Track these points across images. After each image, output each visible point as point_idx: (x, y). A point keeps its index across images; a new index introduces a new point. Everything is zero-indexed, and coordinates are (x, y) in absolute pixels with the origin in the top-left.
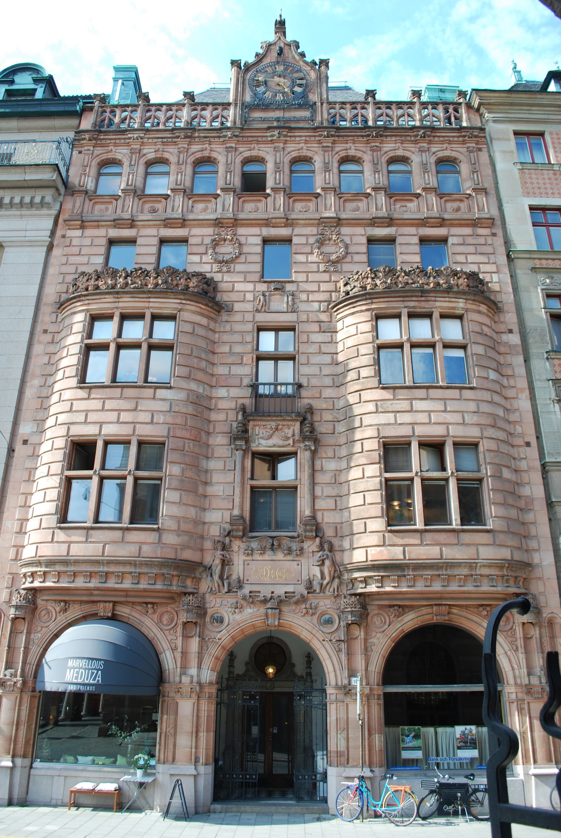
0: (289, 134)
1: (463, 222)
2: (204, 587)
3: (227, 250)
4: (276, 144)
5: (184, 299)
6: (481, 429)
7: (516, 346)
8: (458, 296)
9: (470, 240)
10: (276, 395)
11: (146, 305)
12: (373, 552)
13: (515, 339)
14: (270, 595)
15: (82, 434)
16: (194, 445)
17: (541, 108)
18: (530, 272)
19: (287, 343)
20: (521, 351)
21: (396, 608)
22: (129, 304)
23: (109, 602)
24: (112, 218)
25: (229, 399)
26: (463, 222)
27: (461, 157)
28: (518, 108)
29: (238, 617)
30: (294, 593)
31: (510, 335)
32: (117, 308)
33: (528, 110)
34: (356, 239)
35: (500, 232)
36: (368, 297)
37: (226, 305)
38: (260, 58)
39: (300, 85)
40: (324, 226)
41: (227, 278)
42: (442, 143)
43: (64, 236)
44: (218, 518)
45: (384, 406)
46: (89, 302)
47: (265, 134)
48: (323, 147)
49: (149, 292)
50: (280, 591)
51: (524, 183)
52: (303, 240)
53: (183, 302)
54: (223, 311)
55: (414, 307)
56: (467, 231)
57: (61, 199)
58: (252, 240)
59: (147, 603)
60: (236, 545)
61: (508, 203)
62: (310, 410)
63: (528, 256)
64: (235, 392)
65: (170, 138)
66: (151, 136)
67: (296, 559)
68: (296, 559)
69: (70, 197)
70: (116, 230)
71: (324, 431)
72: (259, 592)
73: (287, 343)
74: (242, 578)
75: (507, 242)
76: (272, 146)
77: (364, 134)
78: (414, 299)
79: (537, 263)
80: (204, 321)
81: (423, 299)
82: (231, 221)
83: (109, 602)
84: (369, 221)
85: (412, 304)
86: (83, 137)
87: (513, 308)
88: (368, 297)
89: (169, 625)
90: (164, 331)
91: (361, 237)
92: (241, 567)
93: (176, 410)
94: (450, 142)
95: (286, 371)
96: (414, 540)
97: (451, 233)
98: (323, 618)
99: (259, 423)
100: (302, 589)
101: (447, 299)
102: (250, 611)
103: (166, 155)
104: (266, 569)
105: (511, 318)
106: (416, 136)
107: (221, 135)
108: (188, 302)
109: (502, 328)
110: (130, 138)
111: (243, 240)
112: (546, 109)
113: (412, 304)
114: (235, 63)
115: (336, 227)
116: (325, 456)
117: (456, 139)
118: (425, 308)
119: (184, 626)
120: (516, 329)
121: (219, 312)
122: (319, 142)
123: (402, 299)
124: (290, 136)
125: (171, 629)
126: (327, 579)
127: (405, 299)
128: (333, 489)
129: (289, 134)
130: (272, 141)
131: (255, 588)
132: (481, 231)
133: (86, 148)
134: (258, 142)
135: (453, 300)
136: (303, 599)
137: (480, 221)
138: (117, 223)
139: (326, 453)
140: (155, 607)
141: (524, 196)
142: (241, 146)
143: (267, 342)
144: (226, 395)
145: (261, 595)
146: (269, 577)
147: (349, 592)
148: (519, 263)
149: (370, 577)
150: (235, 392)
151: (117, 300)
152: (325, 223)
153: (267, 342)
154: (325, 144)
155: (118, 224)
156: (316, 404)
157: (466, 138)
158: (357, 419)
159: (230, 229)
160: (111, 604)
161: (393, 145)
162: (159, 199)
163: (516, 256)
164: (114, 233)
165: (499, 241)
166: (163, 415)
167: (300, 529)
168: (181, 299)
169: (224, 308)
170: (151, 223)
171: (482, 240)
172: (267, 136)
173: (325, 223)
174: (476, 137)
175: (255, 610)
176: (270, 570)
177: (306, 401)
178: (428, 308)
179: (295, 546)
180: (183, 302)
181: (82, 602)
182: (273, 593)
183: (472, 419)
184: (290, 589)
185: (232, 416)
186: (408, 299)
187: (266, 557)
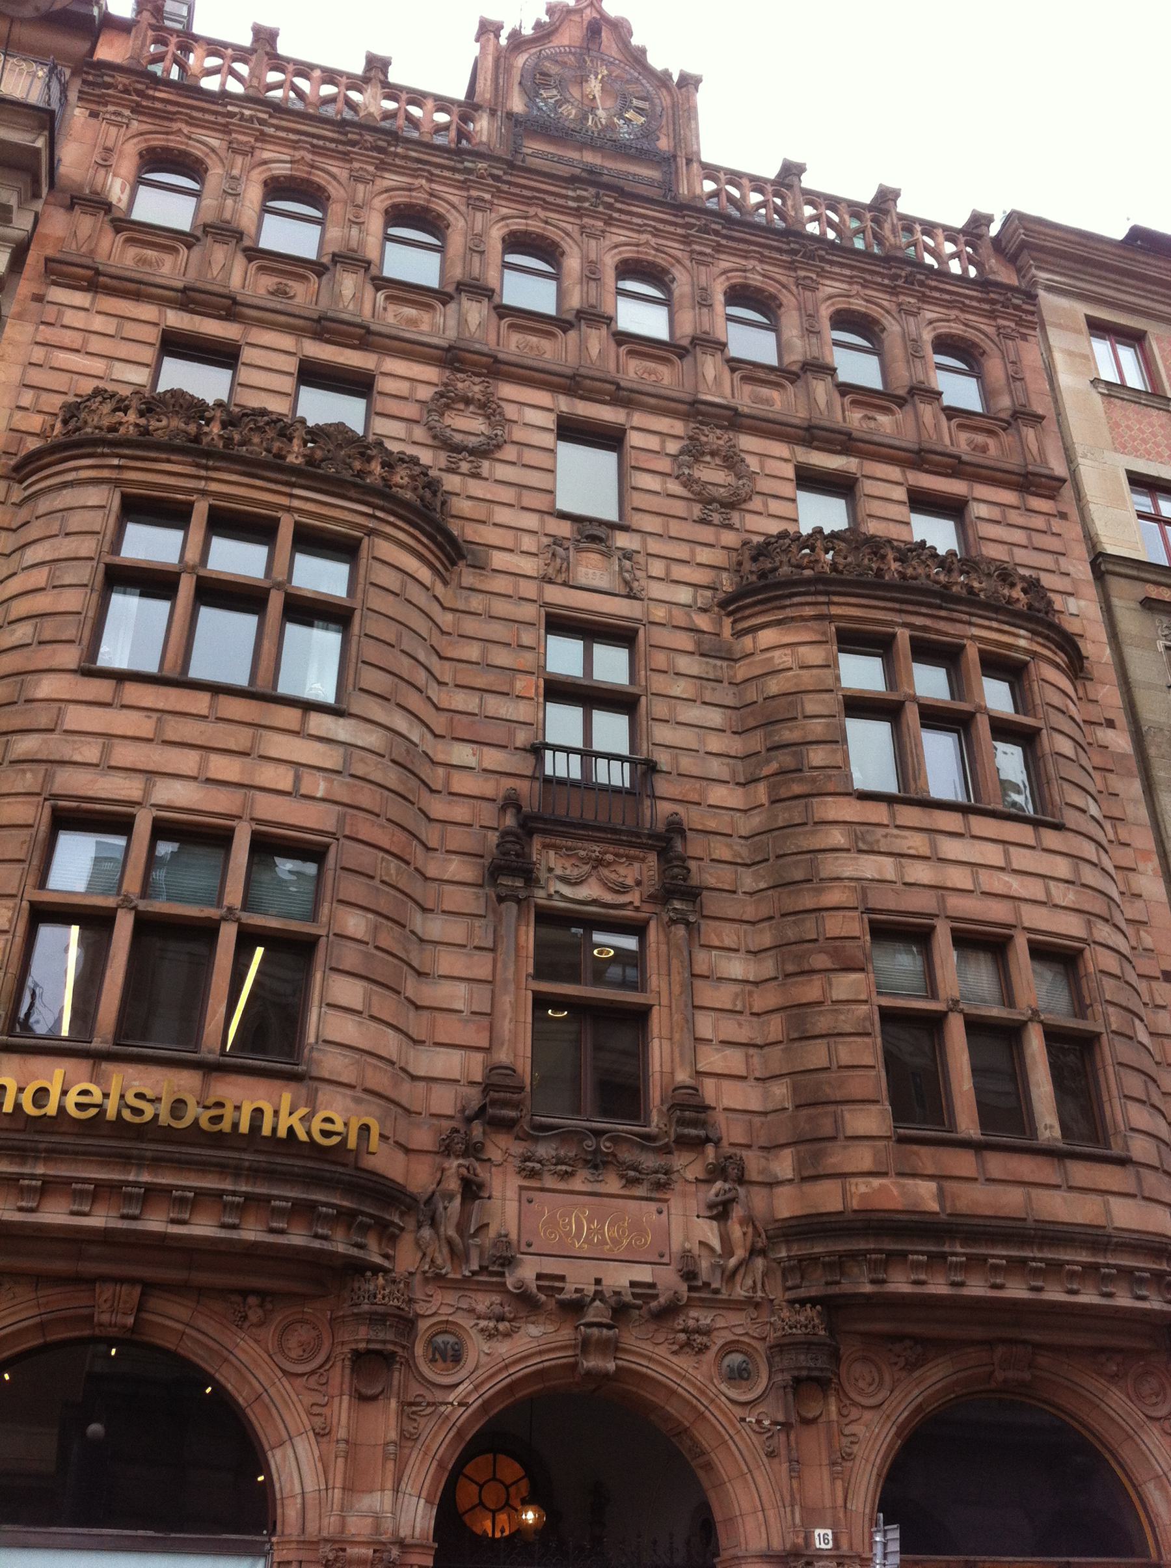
0: (618, 205)
1: (999, 475)
2: (406, 1259)
3: (468, 425)
4: (586, 220)
5: (382, 509)
6: (1089, 922)
7: (1124, 756)
8: (1019, 622)
9: (1014, 517)
10: (586, 786)
11: (285, 501)
12: (863, 1189)
13: (1120, 741)
14: (593, 1288)
15: (90, 793)
16: (398, 869)
17: (1140, 284)
18: (1138, 606)
19: (612, 666)
20: (1135, 770)
21: (908, 1343)
22: (232, 487)
23: (132, 1281)
24: (180, 285)
25: (474, 771)
26: (999, 475)
27: (987, 345)
28: (1097, 272)
29: (504, 1349)
30: (652, 1286)
31: (1110, 732)
32: (204, 493)
33: (1115, 282)
34: (774, 467)
35: (1074, 513)
36: (821, 587)
37: (473, 553)
38: (544, 33)
39: (640, 111)
40: (701, 423)
41: (476, 488)
42: (949, 305)
43: (39, 298)
44: (448, 1069)
45: (869, 838)
46: (123, 462)
47: (564, 192)
48: (692, 252)
49: (293, 470)
50: (620, 1278)
51: (1114, 426)
52: (653, 443)
53: (379, 514)
54: (461, 563)
55: (924, 628)
56: (1009, 497)
57: (38, 206)
58: (532, 416)
59: (244, 1293)
60: (500, 1147)
61: (1085, 456)
62: (676, 828)
63: (1134, 573)
64: (493, 758)
65: (332, 140)
66: (284, 123)
67: (655, 1195)
68: (655, 1195)
69: (62, 210)
70: (186, 317)
71: (711, 881)
72: (562, 1278)
73: (612, 666)
74: (514, 1236)
75: (1090, 539)
76: (578, 221)
77: (785, 247)
78: (924, 610)
79: (1154, 592)
80: (425, 574)
81: (943, 613)
82: (485, 359)
83: (132, 1281)
84: (801, 432)
85: (919, 621)
86: (107, 79)
87: (1112, 675)
88: (821, 587)
89: (314, 1356)
90: (321, 577)
91: (784, 464)
92: (512, 1207)
93: (360, 773)
94: (964, 308)
95: (612, 731)
96: (963, 1163)
97: (977, 495)
98: (727, 1361)
99: (558, 841)
100: (668, 1280)
101: (995, 624)
102: (534, 1330)
103: (319, 178)
104: (577, 1218)
105: (1108, 694)
106: (895, 277)
107: (460, 166)
108: (392, 519)
109: (1094, 713)
110: (231, 115)
111: (510, 411)
112: (1149, 287)
113: (919, 621)
114: (488, 29)
115: (726, 428)
116: (717, 944)
117: (975, 304)
118: (947, 634)
119: (354, 1362)
120: (1121, 719)
121: (454, 564)
122: (686, 240)
123: (897, 606)
124: (620, 211)
125: (313, 1373)
126: (740, 1253)
127: (904, 607)
128: (740, 1025)
129: (618, 205)
130: (578, 209)
131: (551, 1267)
132: (1036, 503)
133: (111, 108)
134: (546, 206)
135: (1006, 628)
136: (671, 1310)
137: (1037, 479)
138: (189, 299)
139: (719, 936)
140: (269, 1306)
141: (1115, 450)
142: (503, 203)
143: (564, 657)
144: (471, 761)
145: (570, 1286)
146: (588, 1241)
147: (790, 1295)
148: (1117, 586)
149: (853, 1255)
150: (493, 758)
151: (203, 473)
152: (703, 414)
153: (564, 657)
154: (697, 248)
155: (194, 302)
156: (693, 818)
157: (998, 307)
158: (127, 1115)
159: (477, 380)
160: (138, 1290)
161: (845, 286)
162: (301, 271)
163: (1111, 567)
164: (176, 319)
165: (1072, 530)
166: (325, 779)
167: (656, 1121)
168: (375, 507)
169: (463, 557)
170: (282, 319)
171: (1039, 522)
172: (566, 197)
173: (703, 414)
174: (1017, 308)
175: (551, 1328)
176: (590, 1222)
177: (665, 808)
178: (953, 636)
179: (649, 1161)
180: (379, 514)
181: (39, 1280)
182: (598, 1281)
183: (1065, 896)
184: (643, 1274)
185: (488, 814)
186: (910, 608)
187: (577, 1184)
